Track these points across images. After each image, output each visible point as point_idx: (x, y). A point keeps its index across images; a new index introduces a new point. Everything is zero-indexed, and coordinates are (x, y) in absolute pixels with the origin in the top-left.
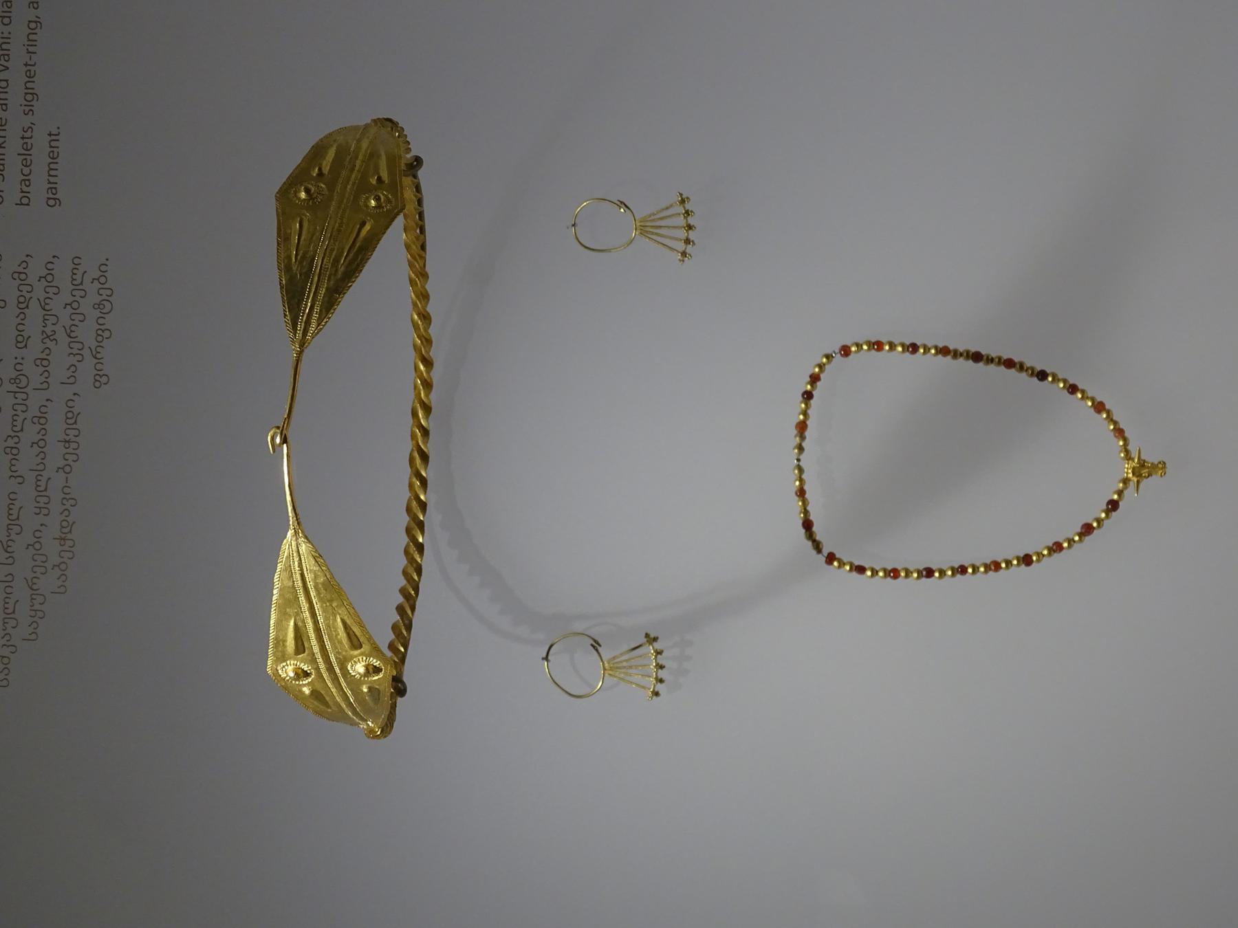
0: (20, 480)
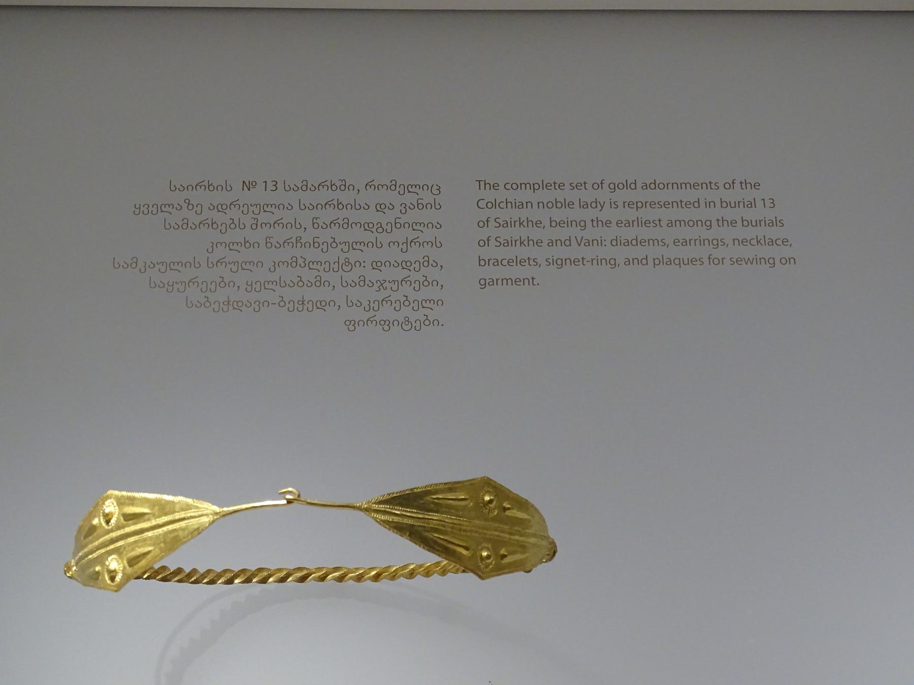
0: (272, 270)
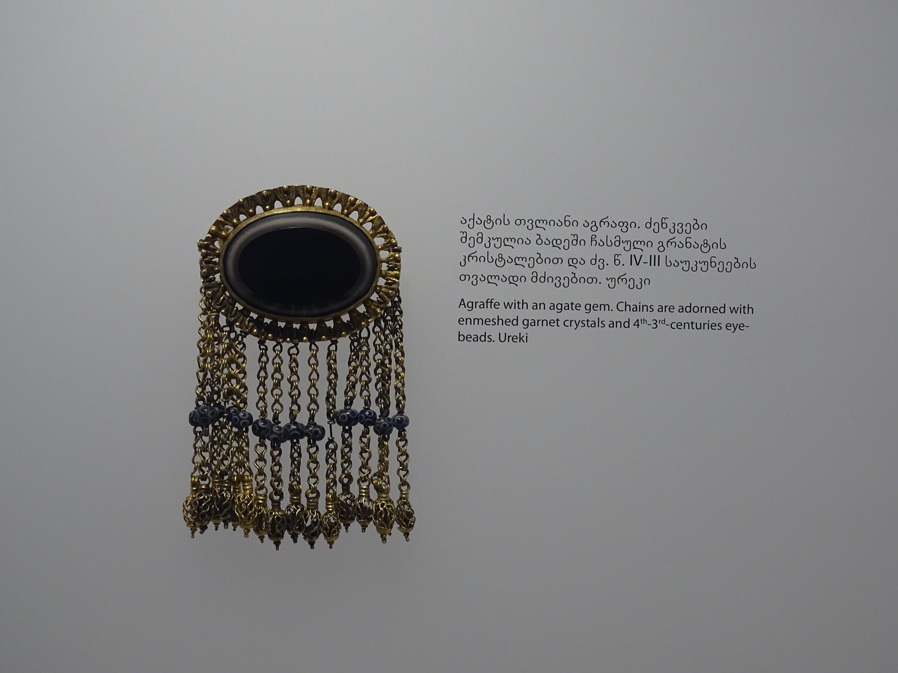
0: (463, 264)
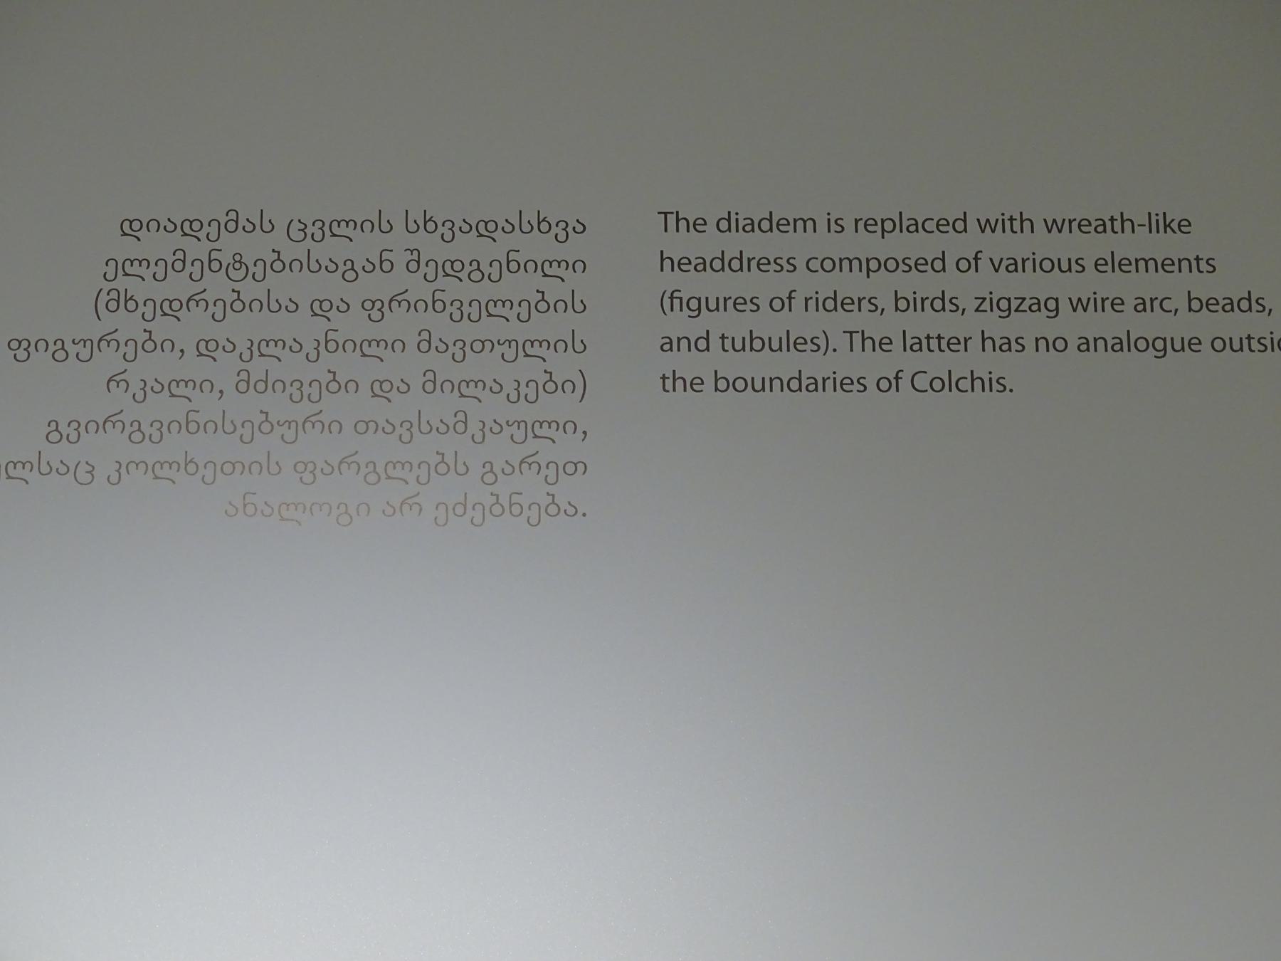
0: (114, 479)
